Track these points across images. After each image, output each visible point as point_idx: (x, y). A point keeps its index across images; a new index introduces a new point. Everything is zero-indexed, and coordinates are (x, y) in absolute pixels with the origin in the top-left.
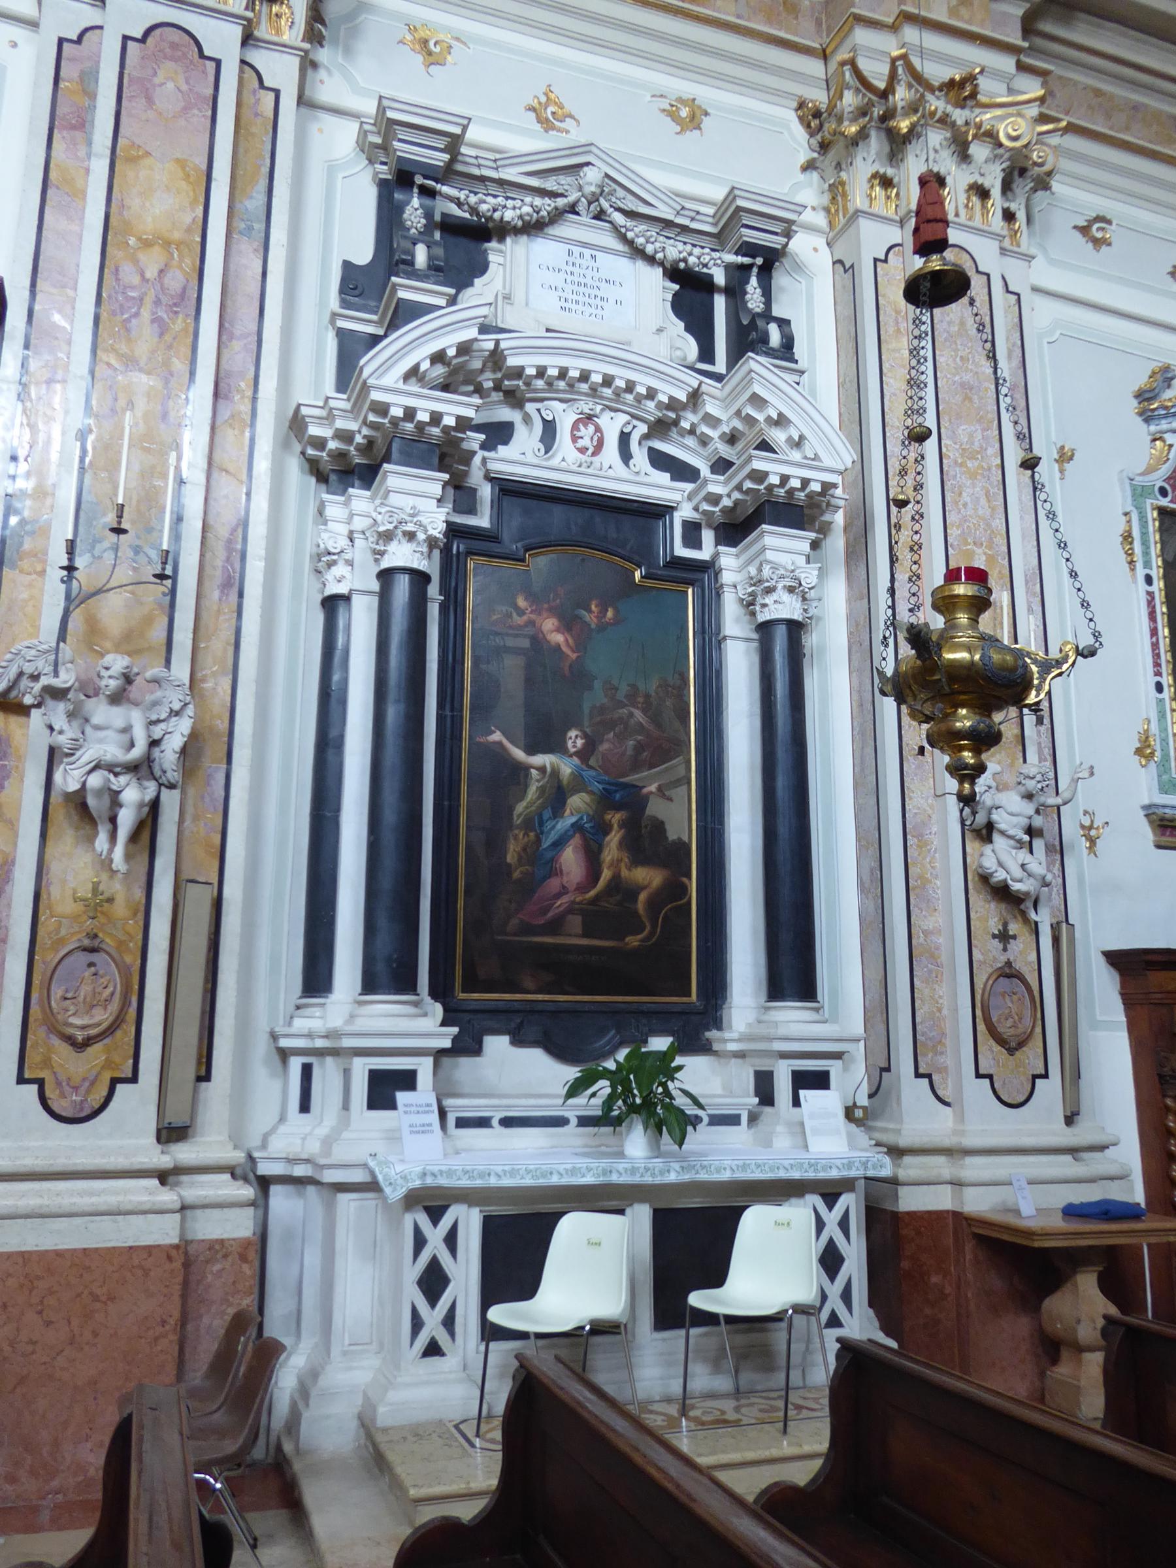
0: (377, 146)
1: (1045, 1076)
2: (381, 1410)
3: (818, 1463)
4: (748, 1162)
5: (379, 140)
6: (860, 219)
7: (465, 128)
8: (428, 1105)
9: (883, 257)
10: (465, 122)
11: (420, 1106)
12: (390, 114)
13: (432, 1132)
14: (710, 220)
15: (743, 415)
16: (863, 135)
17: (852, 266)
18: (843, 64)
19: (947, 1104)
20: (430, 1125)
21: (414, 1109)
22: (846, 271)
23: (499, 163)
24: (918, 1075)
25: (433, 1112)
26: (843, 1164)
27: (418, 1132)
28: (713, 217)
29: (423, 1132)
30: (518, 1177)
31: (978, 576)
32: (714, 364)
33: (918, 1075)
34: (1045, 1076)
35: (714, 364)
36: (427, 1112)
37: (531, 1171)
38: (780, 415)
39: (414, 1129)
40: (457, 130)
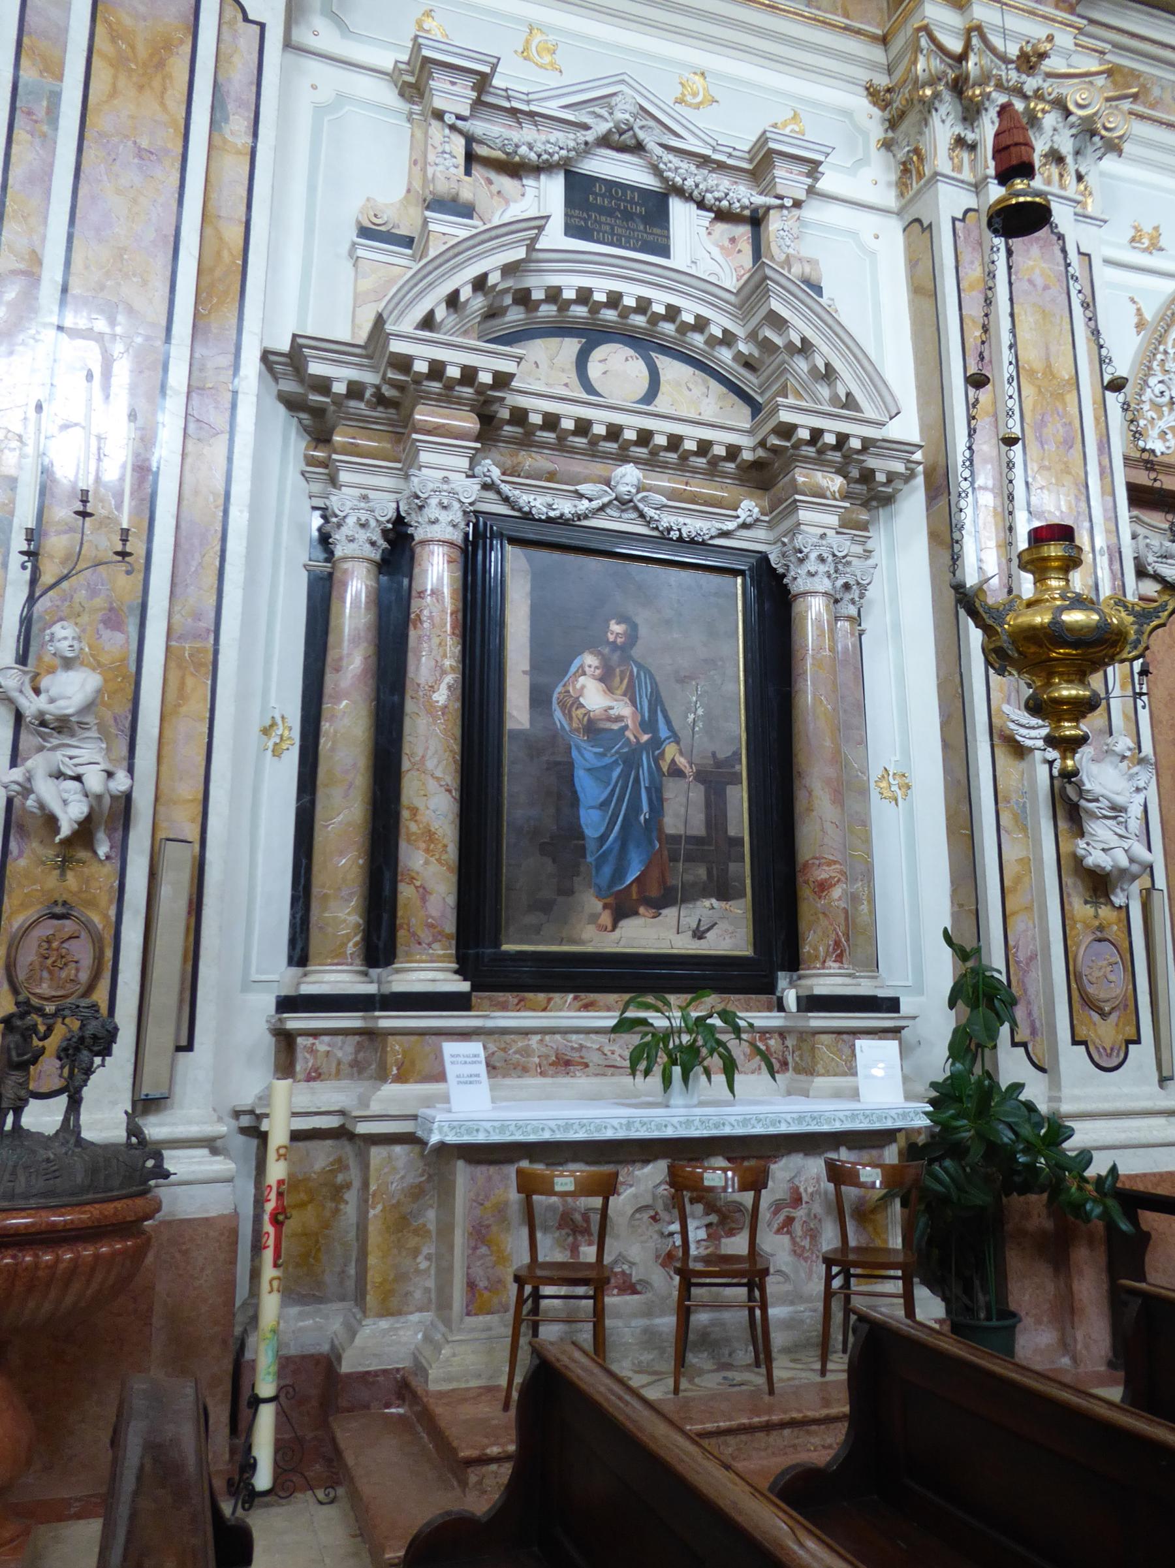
0: (410, 85)
1: (1138, 1041)
2: (433, 1373)
3: (832, 1452)
4: (691, 1118)
5: (412, 80)
6: (940, 184)
7: (494, 67)
8: (475, 1056)
9: (960, 216)
10: (495, 61)
11: (468, 1056)
12: (426, 53)
13: (480, 1082)
14: (747, 156)
15: (760, 337)
16: (936, 95)
17: (930, 225)
18: (919, 29)
19: (1042, 1070)
20: (478, 1076)
21: (459, 1059)
22: (924, 230)
23: (531, 97)
24: (1075, 1042)
25: (480, 1062)
26: (621, 1124)
27: (466, 1083)
28: (749, 152)
29: (471, 1083)
30: (508, 1133)
31: (1064, 533)
32: (668, 257)
33: (1075, 1042)
34: (1138, 1041)
35: (668, 257)
36: (474, 1062)
37: (454, 1128)
38: (804, 340)
39: (462, 1080)
40: (487, 70)
